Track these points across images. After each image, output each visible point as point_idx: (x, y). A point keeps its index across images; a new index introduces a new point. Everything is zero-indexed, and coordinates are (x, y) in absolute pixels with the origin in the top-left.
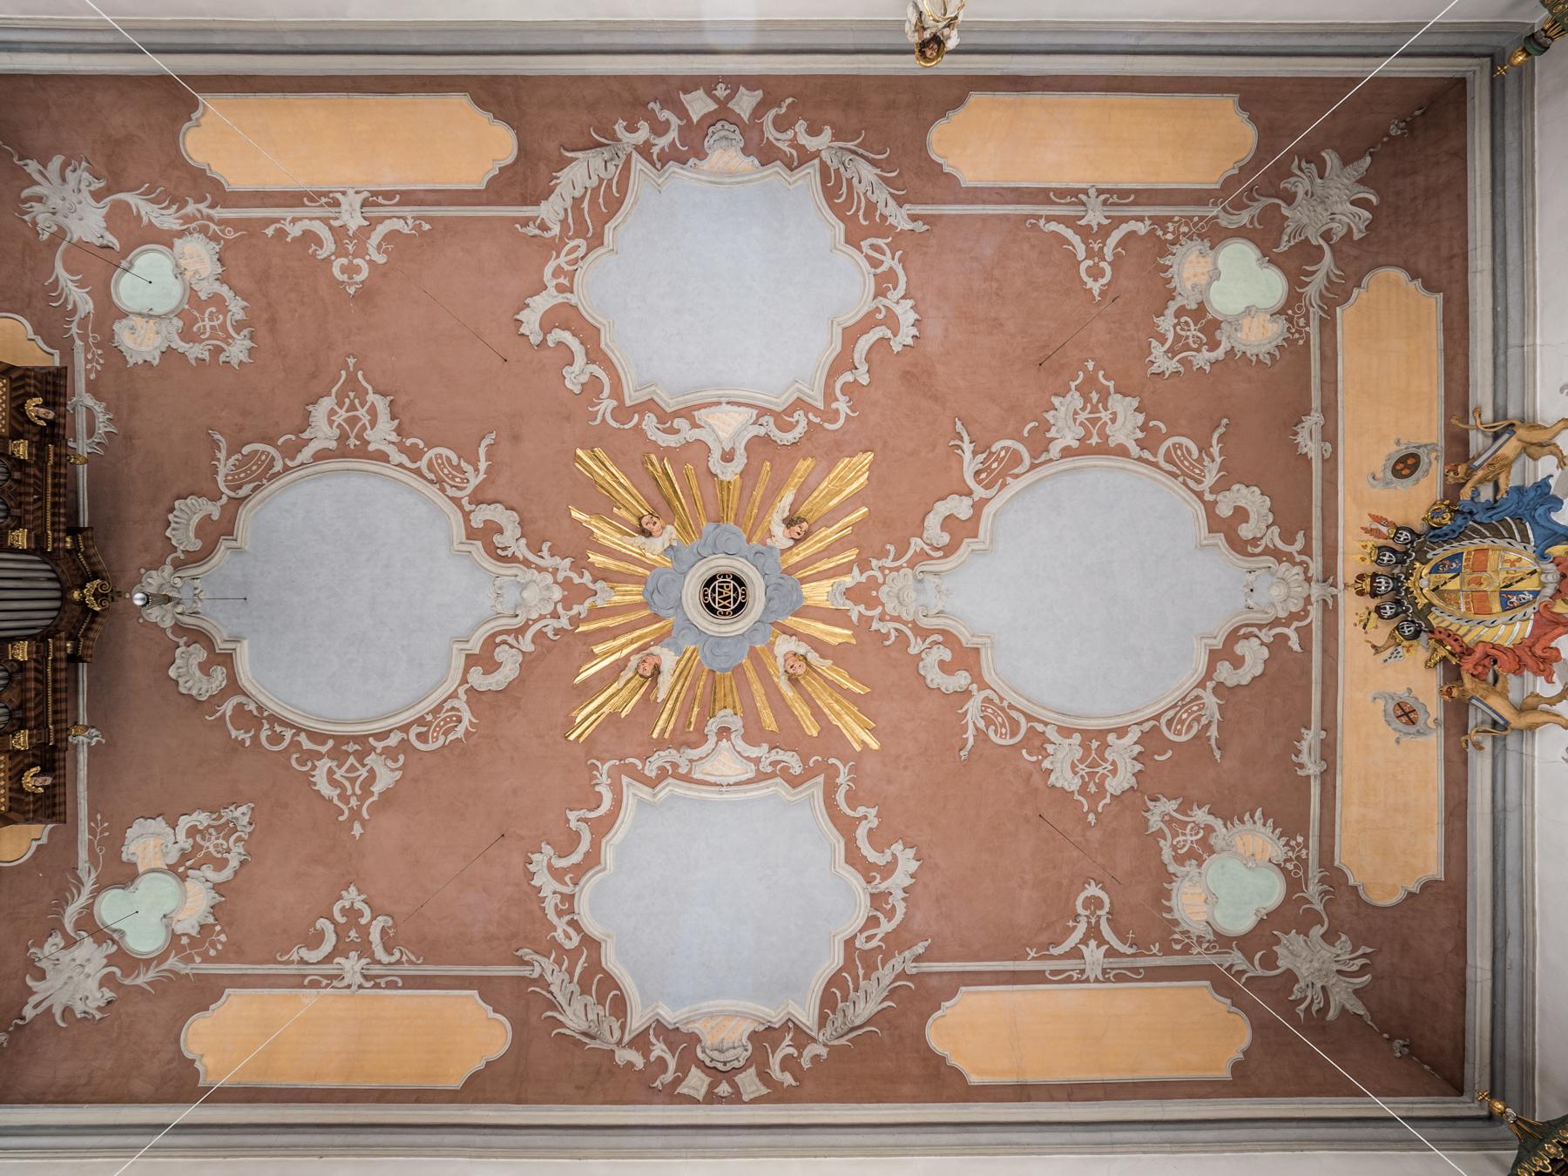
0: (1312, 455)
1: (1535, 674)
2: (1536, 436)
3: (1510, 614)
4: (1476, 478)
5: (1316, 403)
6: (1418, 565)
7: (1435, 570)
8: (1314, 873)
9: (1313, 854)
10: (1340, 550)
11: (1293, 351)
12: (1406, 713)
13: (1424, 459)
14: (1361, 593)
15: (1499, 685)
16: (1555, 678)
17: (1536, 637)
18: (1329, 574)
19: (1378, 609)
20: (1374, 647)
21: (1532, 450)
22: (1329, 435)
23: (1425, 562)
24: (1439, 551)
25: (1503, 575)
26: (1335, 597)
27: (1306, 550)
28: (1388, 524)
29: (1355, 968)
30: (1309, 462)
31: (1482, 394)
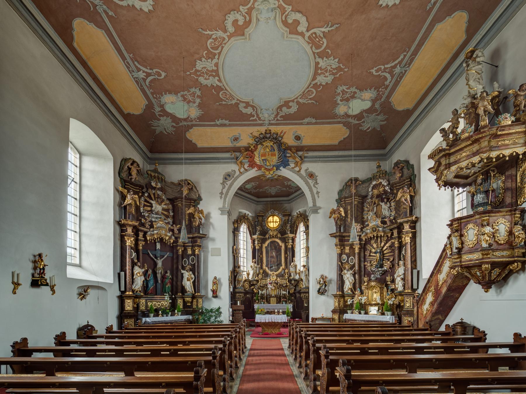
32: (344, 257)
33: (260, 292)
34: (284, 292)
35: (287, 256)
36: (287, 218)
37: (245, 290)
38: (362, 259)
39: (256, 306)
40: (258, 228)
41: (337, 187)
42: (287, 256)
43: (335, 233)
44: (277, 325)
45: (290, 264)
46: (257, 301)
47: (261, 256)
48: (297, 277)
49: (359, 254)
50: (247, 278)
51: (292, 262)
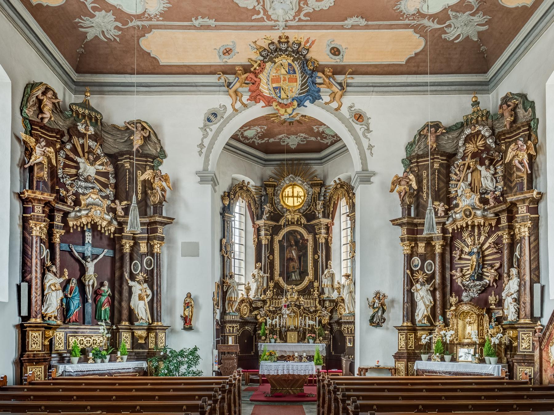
0: (346, 22)
1: (250, 96)
2: (337, 96)
3: (272, 89)
4: (325, 79)
5: (370, 23)
6: (292, 58)
7: (290, 65)
8: (146, 23)
9: (154, 22)
10: (300, 31)
11: (400, 15)
12: (227, 52)
13: (337, 57)
14: (280, 37)
15: (244, 85)
16: (249, 101)
17: (264, 97)
18: (287, 27)
19: (273, 43)
20: (256, 41)
21: (333, 95)
22: (353, 27)
23: (293, 61)
24: (298, 66)
25: (287, 88)
26: (278, 29)
27: (300, 20)
28: (310, 47)
29: (108, 36)
30: (343, 21)
31: (358, 79)
32: (417, 260)
33: (269, 321)
34: (311, 322)
36: (317, 190)
37: (241, 317)
38: (448, 265)
41: (405, 137)
43: (400, 219)
45: (323, 273)
46: (263, 338)
48: (335, 295)
49: (442, 255)
51: (327, 268)
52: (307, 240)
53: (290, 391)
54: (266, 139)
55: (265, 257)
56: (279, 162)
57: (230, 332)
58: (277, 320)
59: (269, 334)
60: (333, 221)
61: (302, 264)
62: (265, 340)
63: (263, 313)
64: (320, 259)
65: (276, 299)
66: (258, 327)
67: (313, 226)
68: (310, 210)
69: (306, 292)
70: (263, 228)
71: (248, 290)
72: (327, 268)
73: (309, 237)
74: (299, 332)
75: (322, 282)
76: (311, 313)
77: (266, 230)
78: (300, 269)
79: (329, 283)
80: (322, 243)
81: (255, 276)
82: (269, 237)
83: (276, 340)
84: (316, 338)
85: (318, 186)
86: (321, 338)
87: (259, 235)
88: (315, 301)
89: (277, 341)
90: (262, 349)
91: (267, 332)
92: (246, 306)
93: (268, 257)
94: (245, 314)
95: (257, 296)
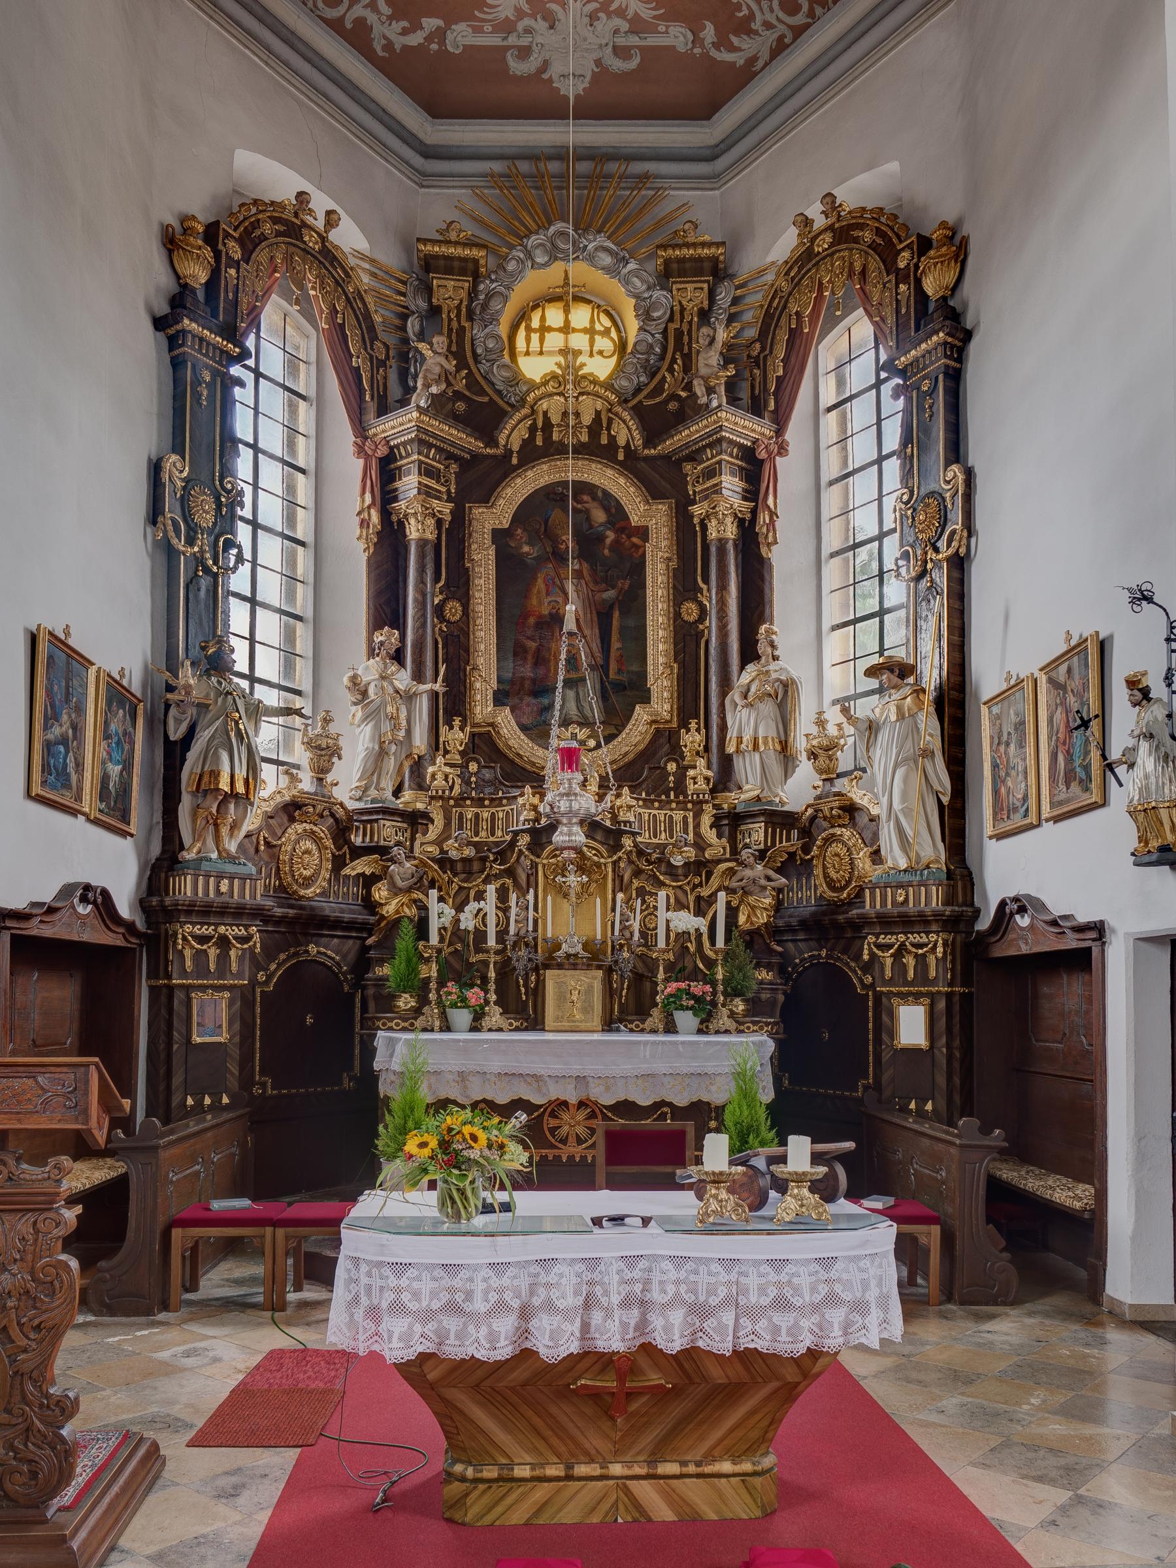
33: (440, 914)
34: (685, 921)
35: (690, 611)
36: (693, 294)
37: (283, 893)
39: (398, 1052)
40: (433, 356)
42: (690, 611)
44: (725, 1395)
45: (726, 685)
46: (406, 1002)
47: (454, 610)
48: (798, 790)
50: (307, 784)
51: (749, 654)
52: (643, 533)
53: (646, 1492)
54: (431, 23)
55: (421, 604)
56: (497, 167)
57: (201, 968)
58: (490, 904)
59: (441, 984)
60: (779, 432)
61: (616, 645)
62: (417, 1012)
63: (402, 870)
64: (712, 622)
65: (479, 802)
66: (378, 945)
67: (673, 464)
68: (658, 390)
69: (648, 773)
70: (410, 461)
71: (325, 753)
72: (749, 654)
73: (652, 517)
74: (609, 971)
75: (723, 728)
76: (672, 871)
77: (427, 471)
78: (605, 668)
79: (768, 730)
80: (722, 542)
81: (364, 694)
82: (445, 509)
83: (479, 1015)
84: (714, 1004)
85: (699, 272)
86: (740, 1006)
87: (386, 497)
88: (698, 815)
89: (486, 1022)
90: (396, 1066)
91: (431, 971)
92: (312, 835)
93: (439, 610)
94: (308, 882)
95: (373, 793)
